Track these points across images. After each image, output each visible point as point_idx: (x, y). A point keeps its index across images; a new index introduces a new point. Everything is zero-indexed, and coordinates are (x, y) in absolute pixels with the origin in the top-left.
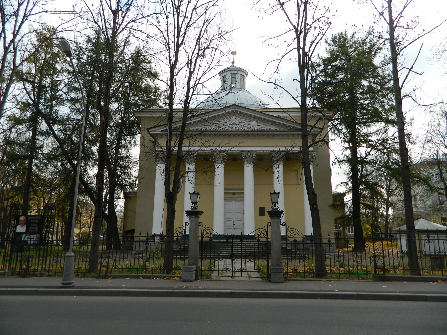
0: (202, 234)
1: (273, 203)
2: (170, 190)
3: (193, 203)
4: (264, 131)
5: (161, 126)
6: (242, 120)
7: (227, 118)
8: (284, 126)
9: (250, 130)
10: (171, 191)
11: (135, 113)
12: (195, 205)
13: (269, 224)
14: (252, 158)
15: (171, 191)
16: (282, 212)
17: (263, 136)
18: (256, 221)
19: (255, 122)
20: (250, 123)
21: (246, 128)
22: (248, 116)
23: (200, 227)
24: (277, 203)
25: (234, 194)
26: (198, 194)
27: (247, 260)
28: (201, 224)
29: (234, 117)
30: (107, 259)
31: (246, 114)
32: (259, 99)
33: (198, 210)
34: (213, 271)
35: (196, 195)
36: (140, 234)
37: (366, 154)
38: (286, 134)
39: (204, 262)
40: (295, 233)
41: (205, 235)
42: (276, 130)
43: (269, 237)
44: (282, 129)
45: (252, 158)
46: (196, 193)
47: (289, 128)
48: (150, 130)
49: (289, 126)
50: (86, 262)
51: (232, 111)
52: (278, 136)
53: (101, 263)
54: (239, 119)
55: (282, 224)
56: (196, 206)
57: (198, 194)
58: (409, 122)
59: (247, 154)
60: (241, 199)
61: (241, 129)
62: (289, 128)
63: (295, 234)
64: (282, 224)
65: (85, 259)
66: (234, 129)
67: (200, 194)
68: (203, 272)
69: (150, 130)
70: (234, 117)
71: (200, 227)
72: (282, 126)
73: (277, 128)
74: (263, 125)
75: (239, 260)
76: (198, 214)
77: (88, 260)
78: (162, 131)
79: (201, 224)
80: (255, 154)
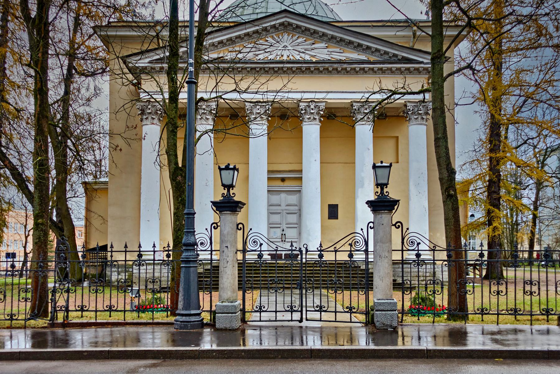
0: (245, 243)
1: (377, 185)
2: (177, 163)
3: (224, 186)
4: (340, 62)
5: (148, 51)
6: (300, 40)
7: (273, 38)
8: (377, 54)
9: (314, 60)
10: (180, 166)
11: (97, 30)
12: (229, 191)
13: (371, 225)
14: (318, 113)
15: (180, 166)
16: (396, 202)
17: (338, 72)
18: (324, 229)
19: (323, 45)
20: (313, 46)
21: (307, 58)
22: (312, 34)
23: (240, 233)
24: (386, 185)
25: (283, 180)
26: (235, 169)
27: (330, 291)
28: (240, 226)
29: (286, 36)
30: (66, 295)
31: (307, 29)
32: (214, 167)
33: (236, 199)
34: (118, 291)
35: (231, 172)
36: (126, 247)
37: (514, 110)
38: (381, 69)
39: (248, 296)
40: (419, 241)
41: (250, 247)
42: (361, 60)
43: (371, 248)
44: (373, 58)
45: (318, 113)
46: (231, 167)
47: (386, 57)
48: (128, 60)
49: (386, 53)
50: (26, 301)
51: (282, 24)
52: (366, 72)
53: (54, 301)
54: (295, 38)
55: (395, 225)
56: (231, 192)
57: (235, 169)
58: (84, 315)
59: (309, 106)
60: (271, 208)
61: (298, 57)
62: (386, 57)
63: (418, 244)
64: (395, 225)
65: (23, 295)
66: (285, 58)
67: (238, 170)
68: (247, 315)
69: (128, 60)
70: (286, 36)
71: (240, 233)
72: (373, 52)
73: (363, 57)
74: (338, 50)
75: (256, 293)
76: (237, 206)
77: (29, 295)
78: (149, 62)
79: (240, 226)
80: (322, 106)
